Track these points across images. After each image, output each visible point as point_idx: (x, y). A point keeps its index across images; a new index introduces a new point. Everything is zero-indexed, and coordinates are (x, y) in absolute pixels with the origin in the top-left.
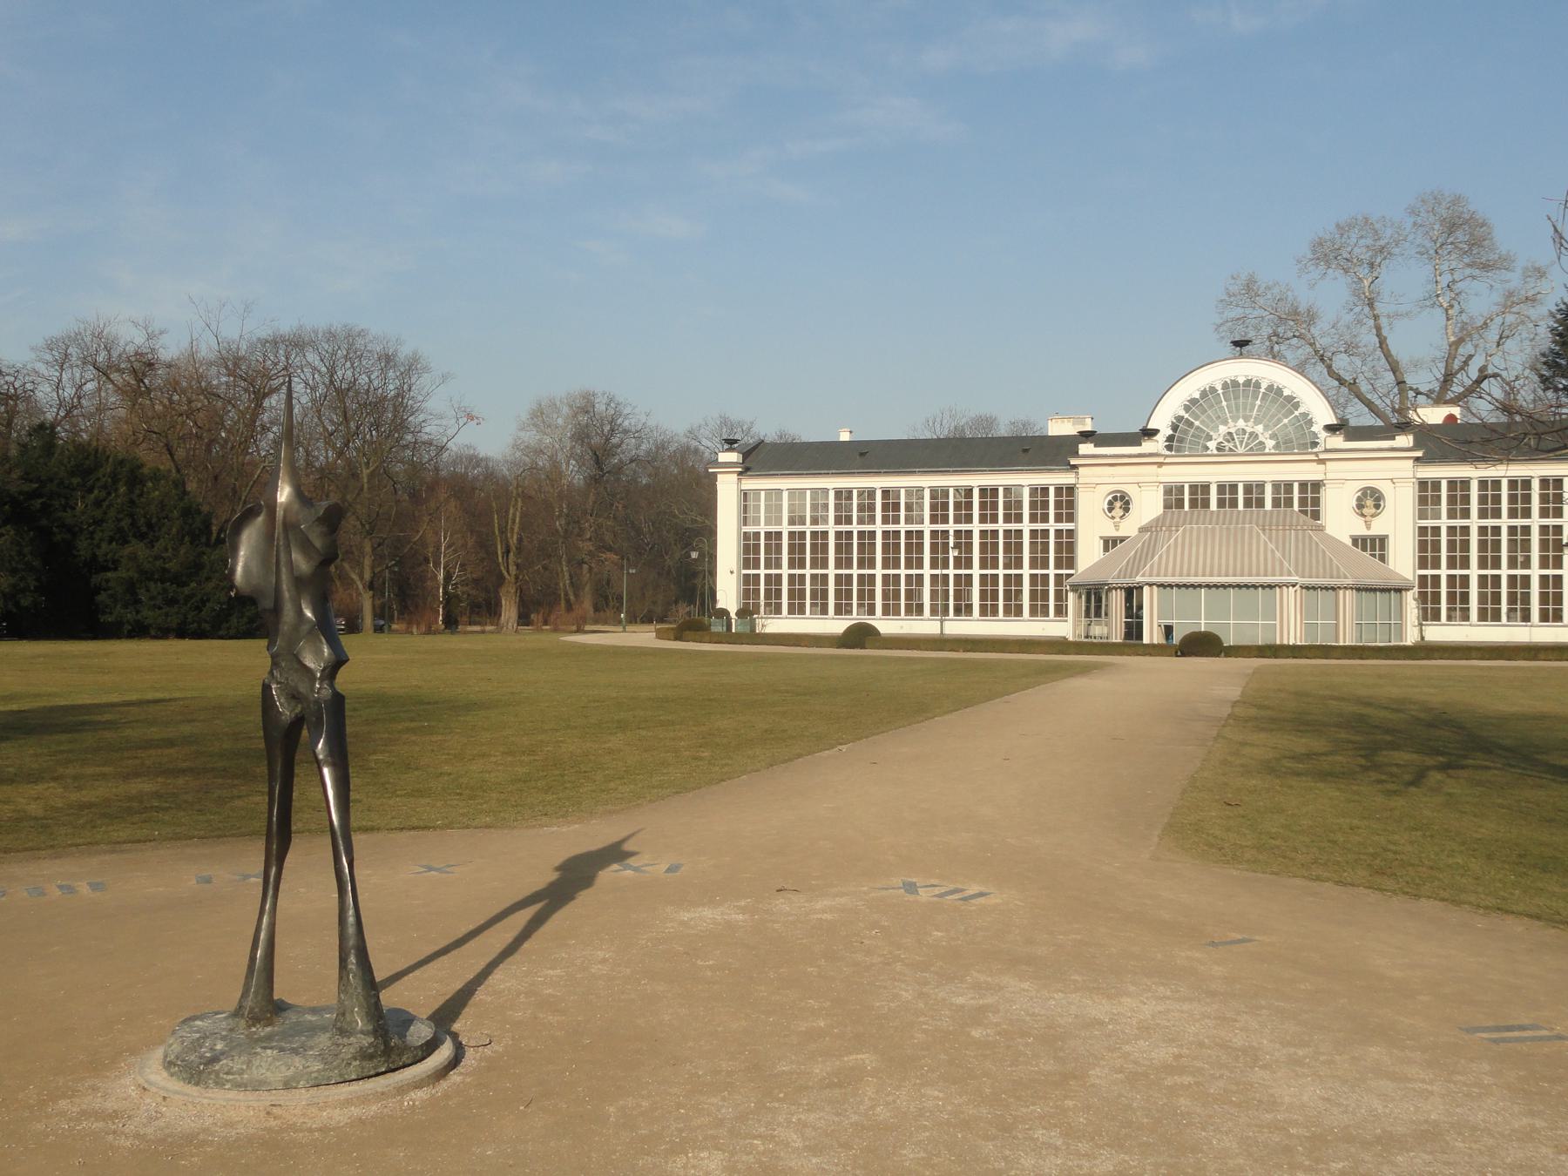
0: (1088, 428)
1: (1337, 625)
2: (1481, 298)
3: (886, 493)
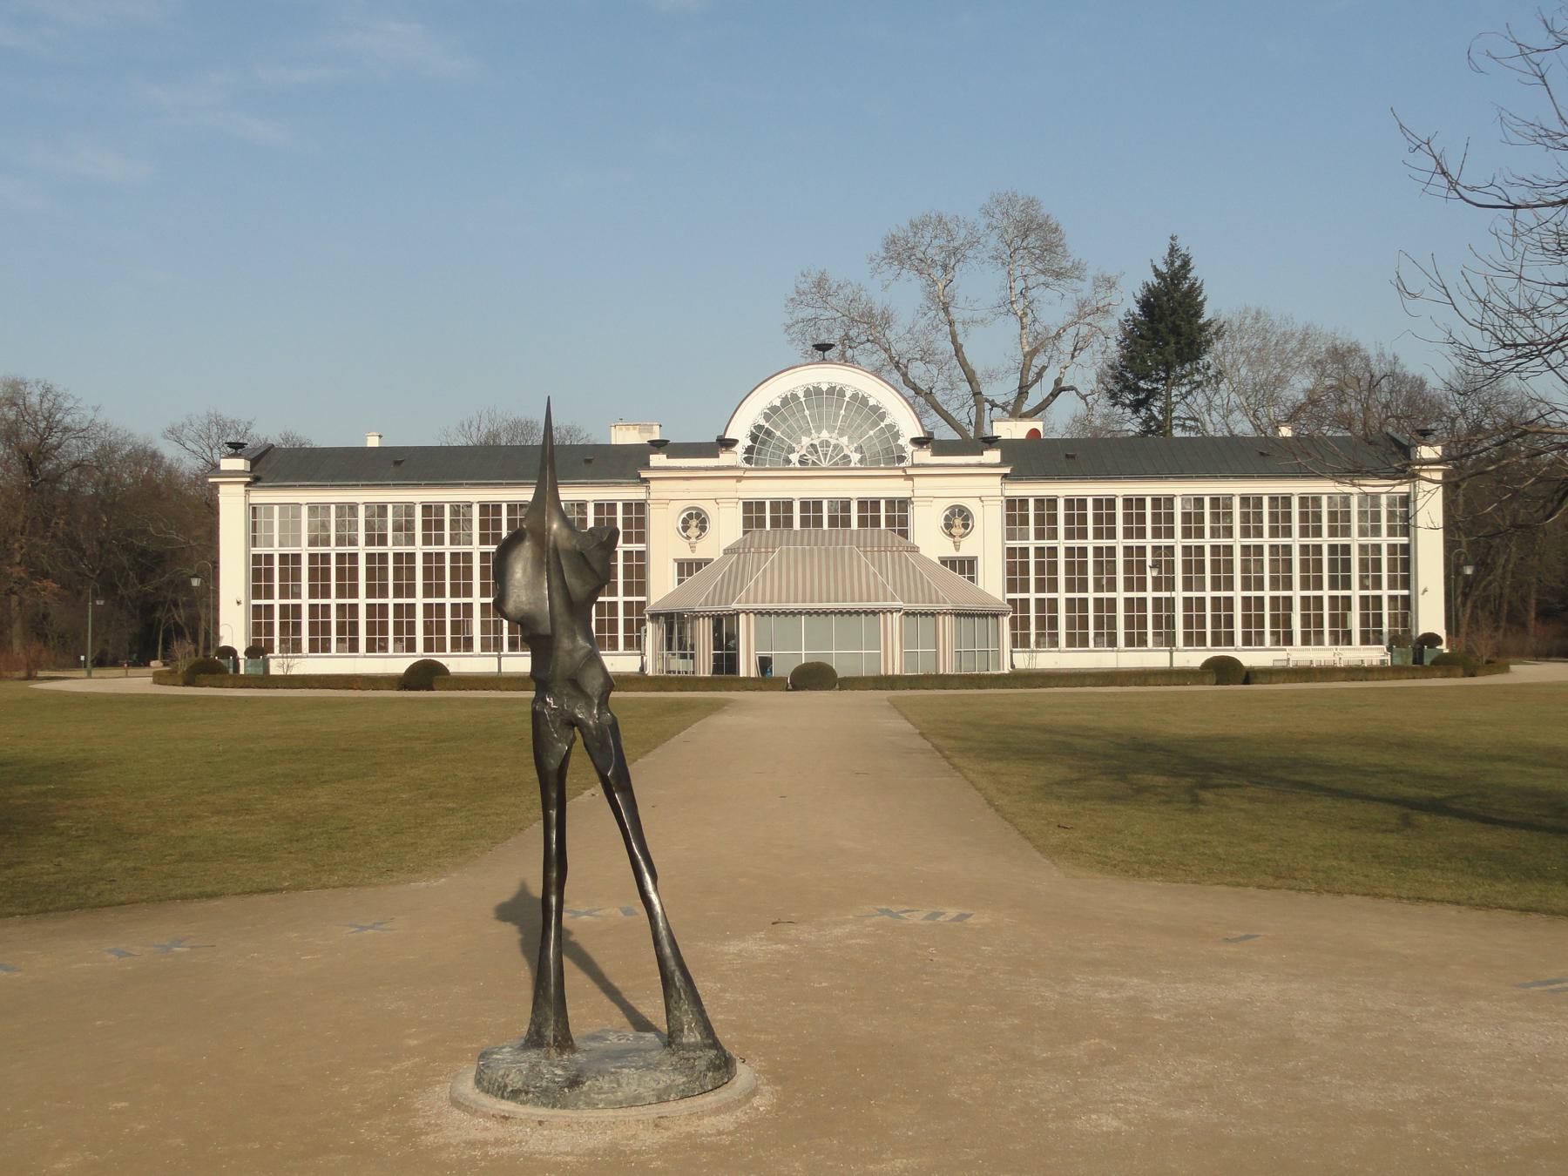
0: (656, 437)
1: (937, 654)
2: (1054, 307)
3: (427, 508)
